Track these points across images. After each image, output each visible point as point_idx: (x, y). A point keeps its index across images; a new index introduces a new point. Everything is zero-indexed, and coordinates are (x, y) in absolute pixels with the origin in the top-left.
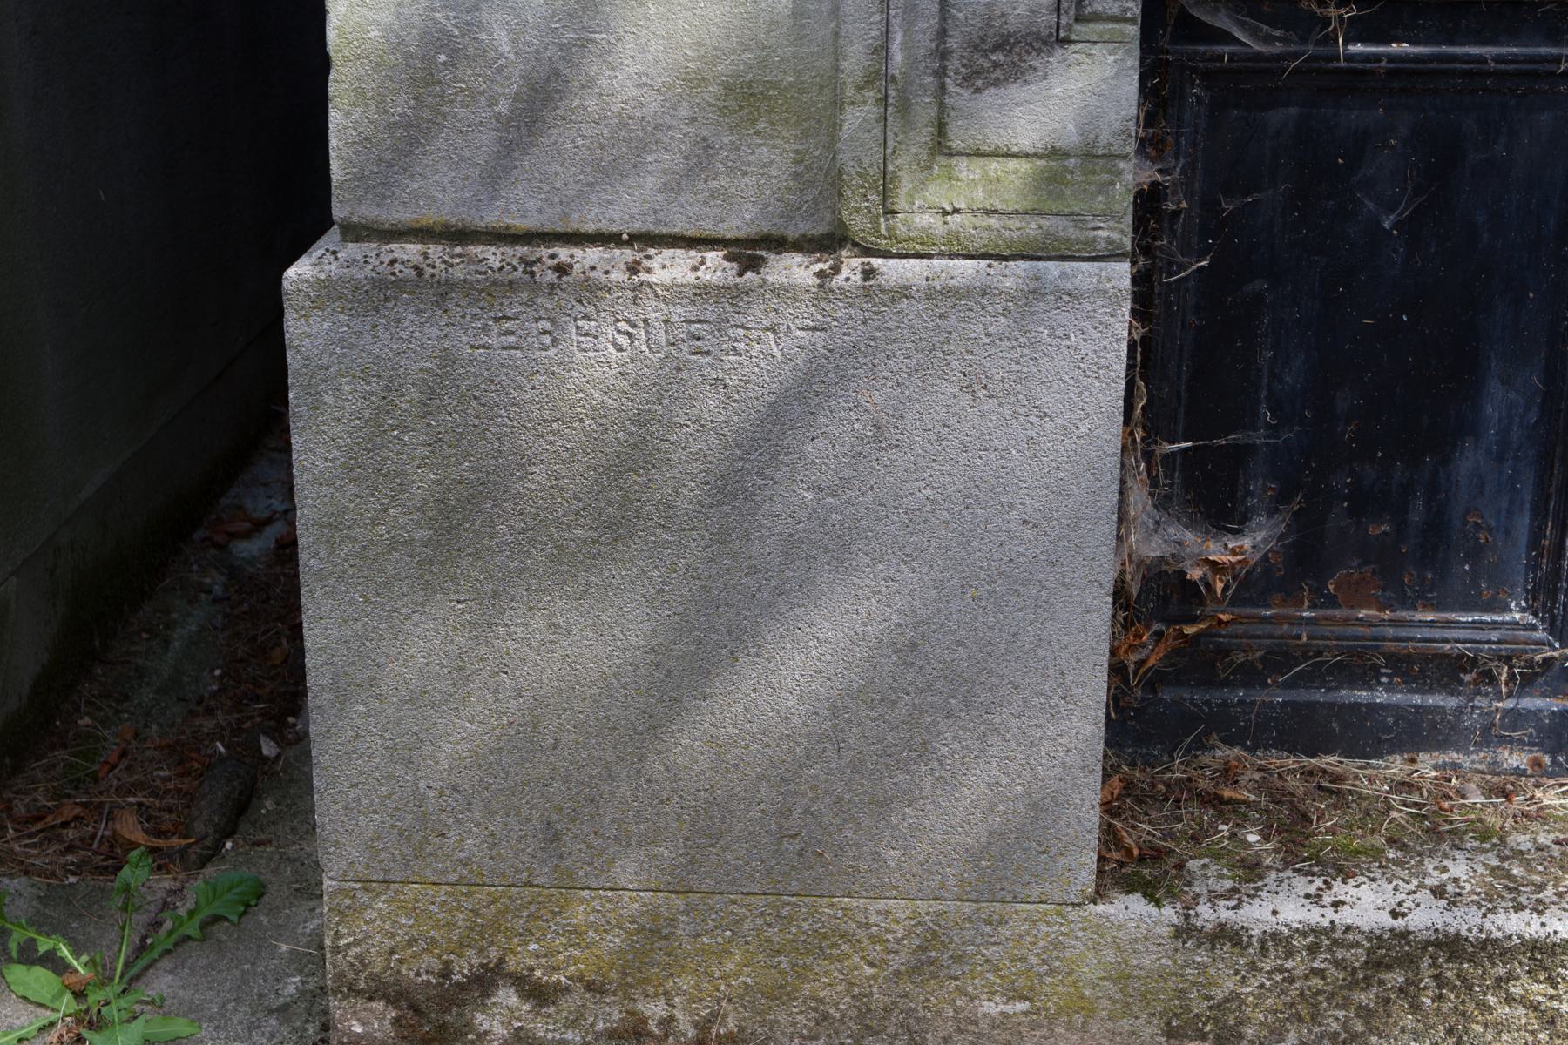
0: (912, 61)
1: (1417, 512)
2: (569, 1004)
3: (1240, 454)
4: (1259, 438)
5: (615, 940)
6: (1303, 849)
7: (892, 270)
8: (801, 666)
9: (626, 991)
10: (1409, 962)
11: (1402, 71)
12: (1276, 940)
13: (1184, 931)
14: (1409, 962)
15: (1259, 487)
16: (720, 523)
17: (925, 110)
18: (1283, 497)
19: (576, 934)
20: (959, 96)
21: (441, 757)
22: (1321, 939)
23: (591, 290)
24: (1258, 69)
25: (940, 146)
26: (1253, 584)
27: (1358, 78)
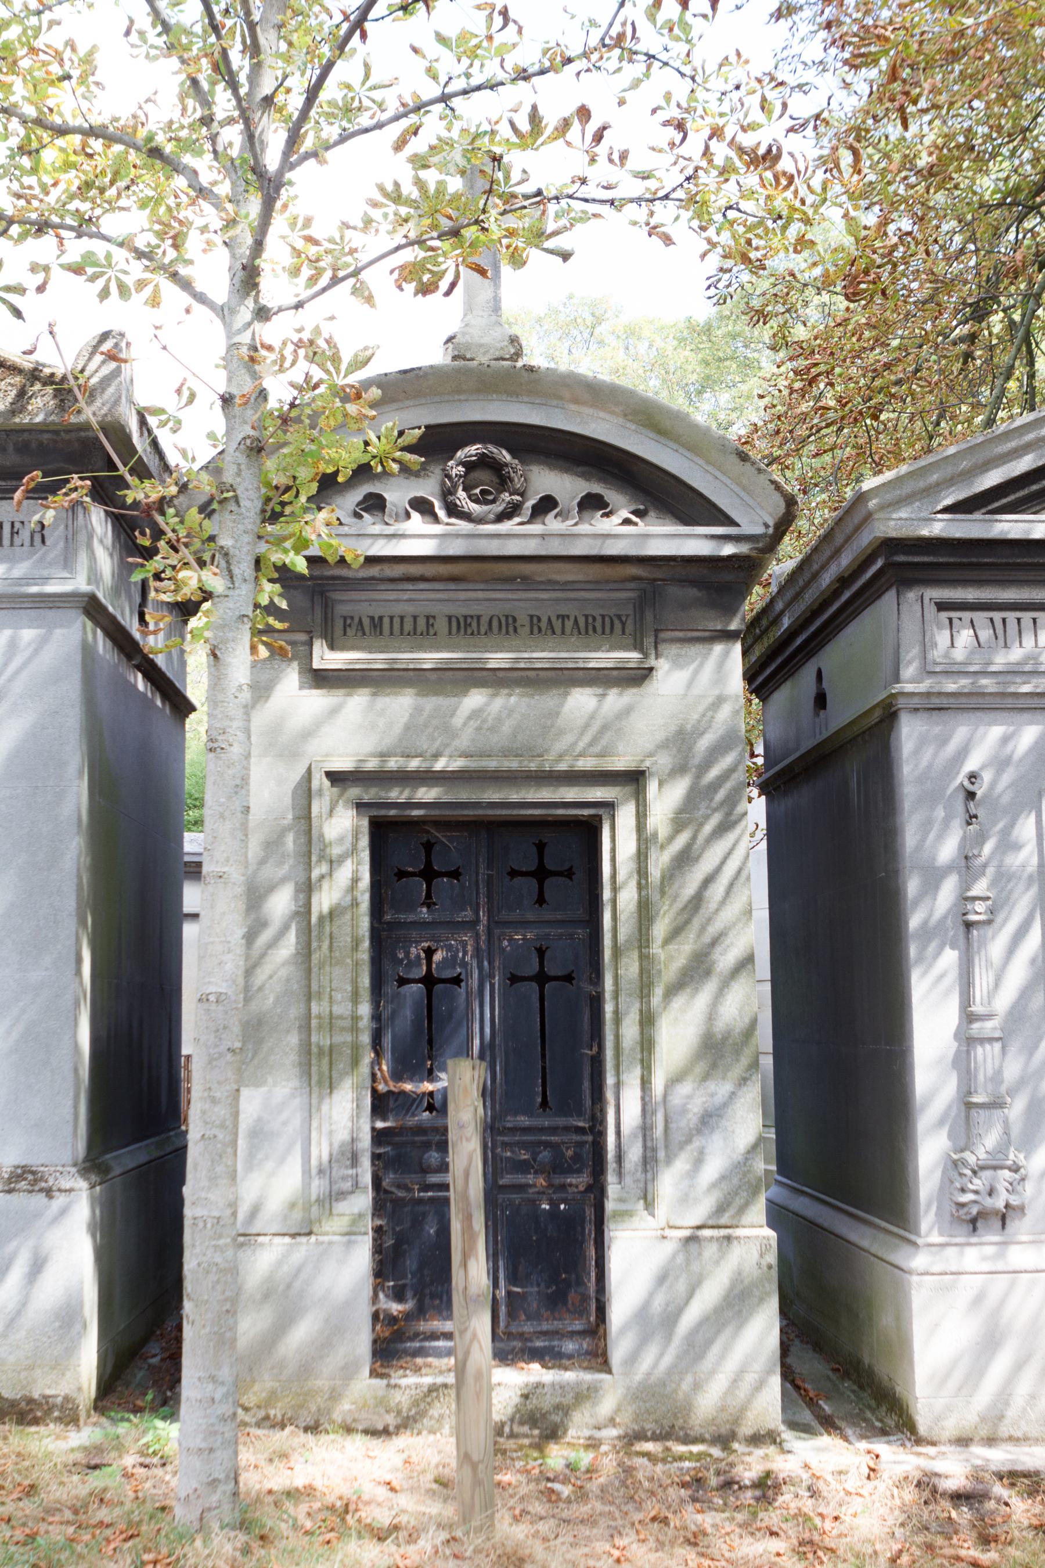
0: (677, 1278)
1: (445, 1298)
2: (252, 1412)
3: (404, 1286)
4: (408, 1281)
5: (264, 1395)
6: (417, 1370)
7: (321, 1238)
8: (302, 1333)
9: (266, 1407)
10: (437, 1390)
11: (431, 1199)
12: (408, 1387)
13: (388, 1385)
14: (437, 1390)
15: (409, 1294)
16: (285, 1299)
17: (327, 1206)
18: (414, 1296)
19: (255, 1393)
20: (334, 1204)
21: (1009, 54)
22: (417, 1386)
23: (262, 1245)
24: (403, 1199)
25: (331, 1214)
26: (408, 1316)
27: (420, 1201)
